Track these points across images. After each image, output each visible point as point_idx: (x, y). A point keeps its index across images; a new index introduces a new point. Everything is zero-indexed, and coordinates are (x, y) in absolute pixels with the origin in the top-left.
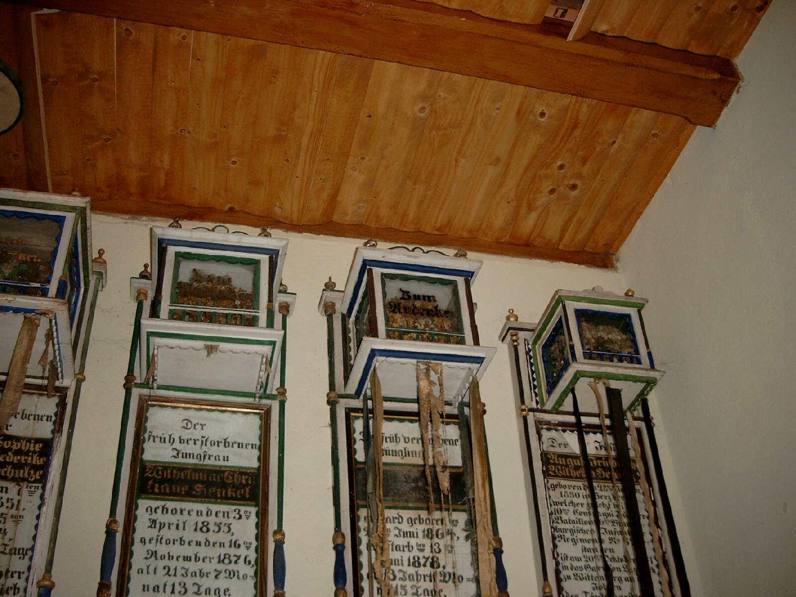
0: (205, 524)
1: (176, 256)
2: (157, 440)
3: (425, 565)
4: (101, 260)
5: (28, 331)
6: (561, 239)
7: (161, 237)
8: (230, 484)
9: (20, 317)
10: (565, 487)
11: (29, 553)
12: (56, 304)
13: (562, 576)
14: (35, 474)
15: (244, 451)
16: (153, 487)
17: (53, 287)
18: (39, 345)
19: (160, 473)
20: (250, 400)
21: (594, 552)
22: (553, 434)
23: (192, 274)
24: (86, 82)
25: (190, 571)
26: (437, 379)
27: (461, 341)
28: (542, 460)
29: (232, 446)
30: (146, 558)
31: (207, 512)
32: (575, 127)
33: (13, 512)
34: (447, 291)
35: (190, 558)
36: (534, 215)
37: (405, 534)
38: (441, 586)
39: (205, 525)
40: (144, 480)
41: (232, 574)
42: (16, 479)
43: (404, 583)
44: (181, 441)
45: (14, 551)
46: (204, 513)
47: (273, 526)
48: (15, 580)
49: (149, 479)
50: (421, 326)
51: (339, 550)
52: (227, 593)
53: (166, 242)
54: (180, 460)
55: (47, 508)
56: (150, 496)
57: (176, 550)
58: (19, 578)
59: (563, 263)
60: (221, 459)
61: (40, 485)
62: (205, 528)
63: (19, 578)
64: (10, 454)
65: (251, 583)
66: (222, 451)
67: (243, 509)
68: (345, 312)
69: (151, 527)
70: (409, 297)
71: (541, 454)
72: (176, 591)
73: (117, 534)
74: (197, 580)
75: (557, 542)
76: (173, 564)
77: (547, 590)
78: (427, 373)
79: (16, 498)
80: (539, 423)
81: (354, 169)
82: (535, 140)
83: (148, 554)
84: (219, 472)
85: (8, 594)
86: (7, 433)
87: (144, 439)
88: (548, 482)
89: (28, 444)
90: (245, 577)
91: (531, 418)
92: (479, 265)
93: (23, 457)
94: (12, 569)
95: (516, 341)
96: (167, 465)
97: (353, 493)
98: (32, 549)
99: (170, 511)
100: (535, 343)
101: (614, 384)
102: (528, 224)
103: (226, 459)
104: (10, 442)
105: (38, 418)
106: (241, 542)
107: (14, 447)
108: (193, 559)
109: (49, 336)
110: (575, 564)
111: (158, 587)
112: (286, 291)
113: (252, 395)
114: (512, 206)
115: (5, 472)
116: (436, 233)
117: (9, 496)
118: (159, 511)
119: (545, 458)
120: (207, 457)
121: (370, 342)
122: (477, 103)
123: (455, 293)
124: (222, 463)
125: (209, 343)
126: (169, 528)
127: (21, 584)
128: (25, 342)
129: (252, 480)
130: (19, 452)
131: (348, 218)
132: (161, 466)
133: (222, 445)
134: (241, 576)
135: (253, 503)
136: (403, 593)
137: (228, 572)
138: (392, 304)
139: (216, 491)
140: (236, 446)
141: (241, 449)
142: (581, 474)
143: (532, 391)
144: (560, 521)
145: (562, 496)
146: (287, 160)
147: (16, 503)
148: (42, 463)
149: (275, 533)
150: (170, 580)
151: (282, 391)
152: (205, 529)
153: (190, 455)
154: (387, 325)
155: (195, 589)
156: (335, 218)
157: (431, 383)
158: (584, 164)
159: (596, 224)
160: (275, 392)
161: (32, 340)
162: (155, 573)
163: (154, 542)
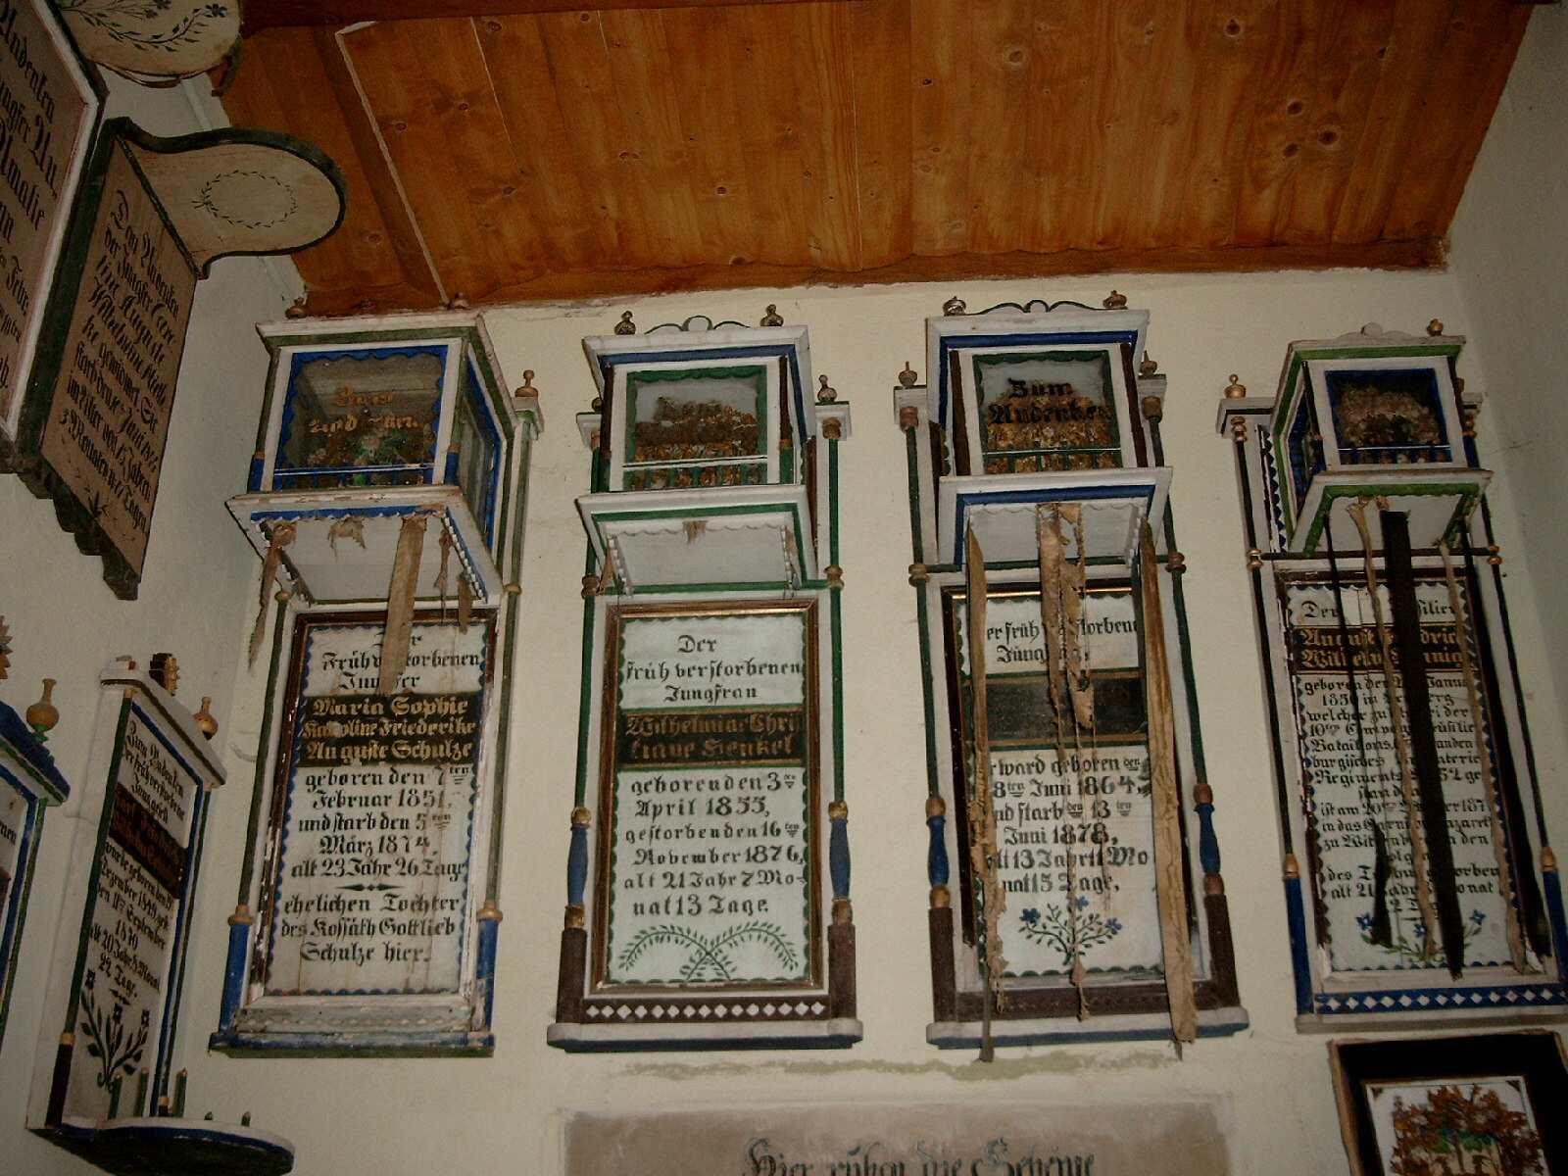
0: (725, 801)
1: (629, 380)
2: (642, 674)
3: (1082, 839)
4: (528, 390)
5: (410, 542)
6: (1331, 226)
7: (600, 353)
8: (760, 734)
9: (396, 522)
10: (1331, 687)
11: (463, 870)
12: (444, 495)
13: (1321, 842)
14: (461, 748)
15: (779, 677)
16: (640, 750)
18: (431, 555)
19: (650, 727)
20: (777, 594)
21: (1382, 796)
22: (1311, 594)
23: (657, 406)
24: (452, 111)
25: (705, 876)
26: (1072, 533)
27: (1116, 461)
28: (1287, 643)
29: (761, 672)
30: (637, 863)
31: (727, 783)
32: (1300, 37)
33: (434, 810)
34: (1093, 369)
35: (704, 857)
36: (1268, 195)
37: (1049, 791)
38: (1112, 870)
39: (725, 802)
40: (625, 742)
41: (772, 877)
42: (435, 760)
43: (1046, 871)
44: (680, 672)
45: (441, 870)
46: (722, 785)
47: (827, 796)
48: (447, 912)
49: (632, 738)
50: (1046, 440)
51: (936, 825)
52: (763, 908)
53: (610, 359)
54: (679, 703)
55: (483, 801)
56: (636, 765)
57: (684, 847)
58: (452, 908)
59: (1340, 271)
60: (744, 694)
61: (470, 766)
62: (723, 808)
63: (452, 908)
65: (799, 887)
66: (743, 682)
67: (782, 772)
68: (936, 420)
69: (640, 813)
70: (1025, 392)
71: (1286, 634)
72: (685, 910)
73: (588, 831)
74: (716, 890)
75: (1313, 784)
76: (677, 869)
77: (1290, 870)
78: (1055, 524)
79: (437, 789)
80: (1282, 581)
81: (926, 168)
82: (1234, 72)
83: (639, 855)
84: (740, 716)
85: (439, 933)
86: (415, 690)
87: (621, 675)
88: (1298, 680)
89: (447, 704)
90: (790, 879)
91: (1267, 569)
92: (1143, 318)
93: (441, 725)
94: (441, 897)
95: (1241, 433)
96: (659, 713)
97: (959, 729)
98: (467, 864)
99: (668, 787)
100: (1278, 432)
101: (1396, 504)
102: (1263, 209)
103: (752, 693)
104: (419, 705)
106: (780, 825)
107: (427, 712)
108: (708, 859)
109: (446, 541)
110: (1347, 819)
111: (657, 906)
112: (833, 399)
113: (783, 585)
114: (1222, 185)
115: (418, 752)
116: (1101, 248)
117: (427, 787)
118: (651, 788)
119: (1295, 640)
120: (721, 695)
121: (955, 485)
122: (1109, 28)
123: (1106, 373)
124: (744, 701)
125: (692, 520)
126: (669, 813)
127: (456, 918)
128: (408, 559)
129: (795, 725)
131: (940, 245)
132: (651, 717)
133: (743, 672)
134: (783, 880)
135: (798, 761)
136: (1046, 888)
137: (763, 874)
138: (995, 408)
139: (738, 747)
140: (766, 671)
141: (774, 675)
142: (1361, 662)
143: (1273, 521)
144: (1321, 748)
145: (1325, 704)
146: (807, 173)
147: (437, 797)
148: (469, 731)
149: (832, 807)
150: (675, 894)
151: (835, 573)
152: (724, 810)
153: (697, 694)
154: (984, 448)
155: (714, 904)
156: (918, 248)
157: (1063, 541)
158: (1336, 97)
159: (1391, 193)
160: (822, 576)
161: (417, 555)
162: (651, 885)
163: (646, 837)
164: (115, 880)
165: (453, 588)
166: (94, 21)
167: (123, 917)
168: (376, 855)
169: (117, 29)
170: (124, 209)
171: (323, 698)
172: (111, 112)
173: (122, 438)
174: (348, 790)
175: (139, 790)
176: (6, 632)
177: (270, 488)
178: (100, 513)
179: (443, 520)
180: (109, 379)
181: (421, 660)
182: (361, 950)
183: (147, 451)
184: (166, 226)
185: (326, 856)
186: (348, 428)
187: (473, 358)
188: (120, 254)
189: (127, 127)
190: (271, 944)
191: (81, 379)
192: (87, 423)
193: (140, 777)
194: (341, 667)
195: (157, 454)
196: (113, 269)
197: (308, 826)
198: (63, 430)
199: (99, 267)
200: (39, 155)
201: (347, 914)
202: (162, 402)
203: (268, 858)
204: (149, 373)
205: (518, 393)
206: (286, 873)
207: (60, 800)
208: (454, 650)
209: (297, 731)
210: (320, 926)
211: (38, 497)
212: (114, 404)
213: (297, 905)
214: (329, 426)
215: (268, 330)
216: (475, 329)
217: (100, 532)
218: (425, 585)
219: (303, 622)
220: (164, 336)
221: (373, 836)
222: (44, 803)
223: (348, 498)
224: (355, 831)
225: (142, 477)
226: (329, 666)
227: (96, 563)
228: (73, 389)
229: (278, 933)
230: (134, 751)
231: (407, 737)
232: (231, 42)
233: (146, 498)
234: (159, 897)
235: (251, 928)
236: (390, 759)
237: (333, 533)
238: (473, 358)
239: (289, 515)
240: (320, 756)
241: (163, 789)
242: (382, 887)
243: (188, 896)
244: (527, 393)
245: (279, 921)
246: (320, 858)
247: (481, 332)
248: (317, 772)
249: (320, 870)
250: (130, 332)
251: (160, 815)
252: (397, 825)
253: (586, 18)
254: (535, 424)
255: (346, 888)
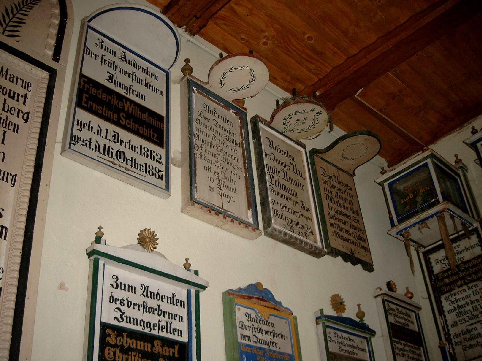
9: (435, 218)
12: (444, 205)
17: (440, 197)
18: (449, 222)
64: (470, 269)
86: (464, 260)
93: (476, 268)
105: (472, 247)
109: (452, 217)
128: (443, 227)
130: (474, 266)
152: (477, 293)
161: (445, 225)
164: (400, 350)
165: (460, 227)
166: (292, 131)
167: (407, 359)
168: (473, 313)
169: (299, 130)
170: (324, 171)
171: (440, 273)
172: (309, 149)
173: (352, 231)
174: (458, 297)
175: (397, 322)
176: (341, 297)
177: (397, 224)
178: (354, 253)
179: (448, 212)
180: (341, 217)
181: (462, 251)
182: (480, 343)
183: (360, 230)
184: (338, 169)
185: (459, 318)
186: (411, 197)
187: (435, 161)
188: (329, 183)
189: (315, 151)
190: (453, 350)
191: (333, 221)
192: (339, 232)
193: (395, 318)
194: (441, 262)
195: (363, 229)
196: (329, 188)
197: (449, 312)
198: (334, 237)
199: (324, 190)
200: (295, 172)
201: (472, 333)
202: (358, 215)
203: (443, 325)
204: (351, 209)
205: (456, 162)
206: (450, 327)
207: (374, 336)
208: (470, 244)
209: (436, 285)
210: (465, 339)
211: (336, 257)
212: (345, 223)
213: (457, 336)
214: (406, 200)
215: (378, 181)
216: (432, 154)
217: (356, 258)
218: (451, 230)
219: (425, 254)
220: (351, 197)
221: (470, 308)
222: (370, 338)
223: (419, 218)
224: (464, 308)
225: (362, 237)
226: (438, 263)
227: (359, 266)
228: (331, 224)
229: (454, 346)
230: (391, 312)
231: (468, 275)
232: (327, 118)
233: (365, 242)
234: (415, 348)
235: (446, 347)
236: (466, 284)
237: (419, 229)
238: (435, 161)
239: (405, 229)
240: (445, 290)
241: (404, 318)
242: (478, 322)
243: (424, 345)
244: (458, 161)
245: (453, 342)
246: (457, 320)
247: (435, 153)
248: (447, 295)
249: (459, 323)
250: (341, 202)
251: (406, 326)
252: (475, 302)
253: (418, 55)
254: (464, 169)
255: (469, 325)
